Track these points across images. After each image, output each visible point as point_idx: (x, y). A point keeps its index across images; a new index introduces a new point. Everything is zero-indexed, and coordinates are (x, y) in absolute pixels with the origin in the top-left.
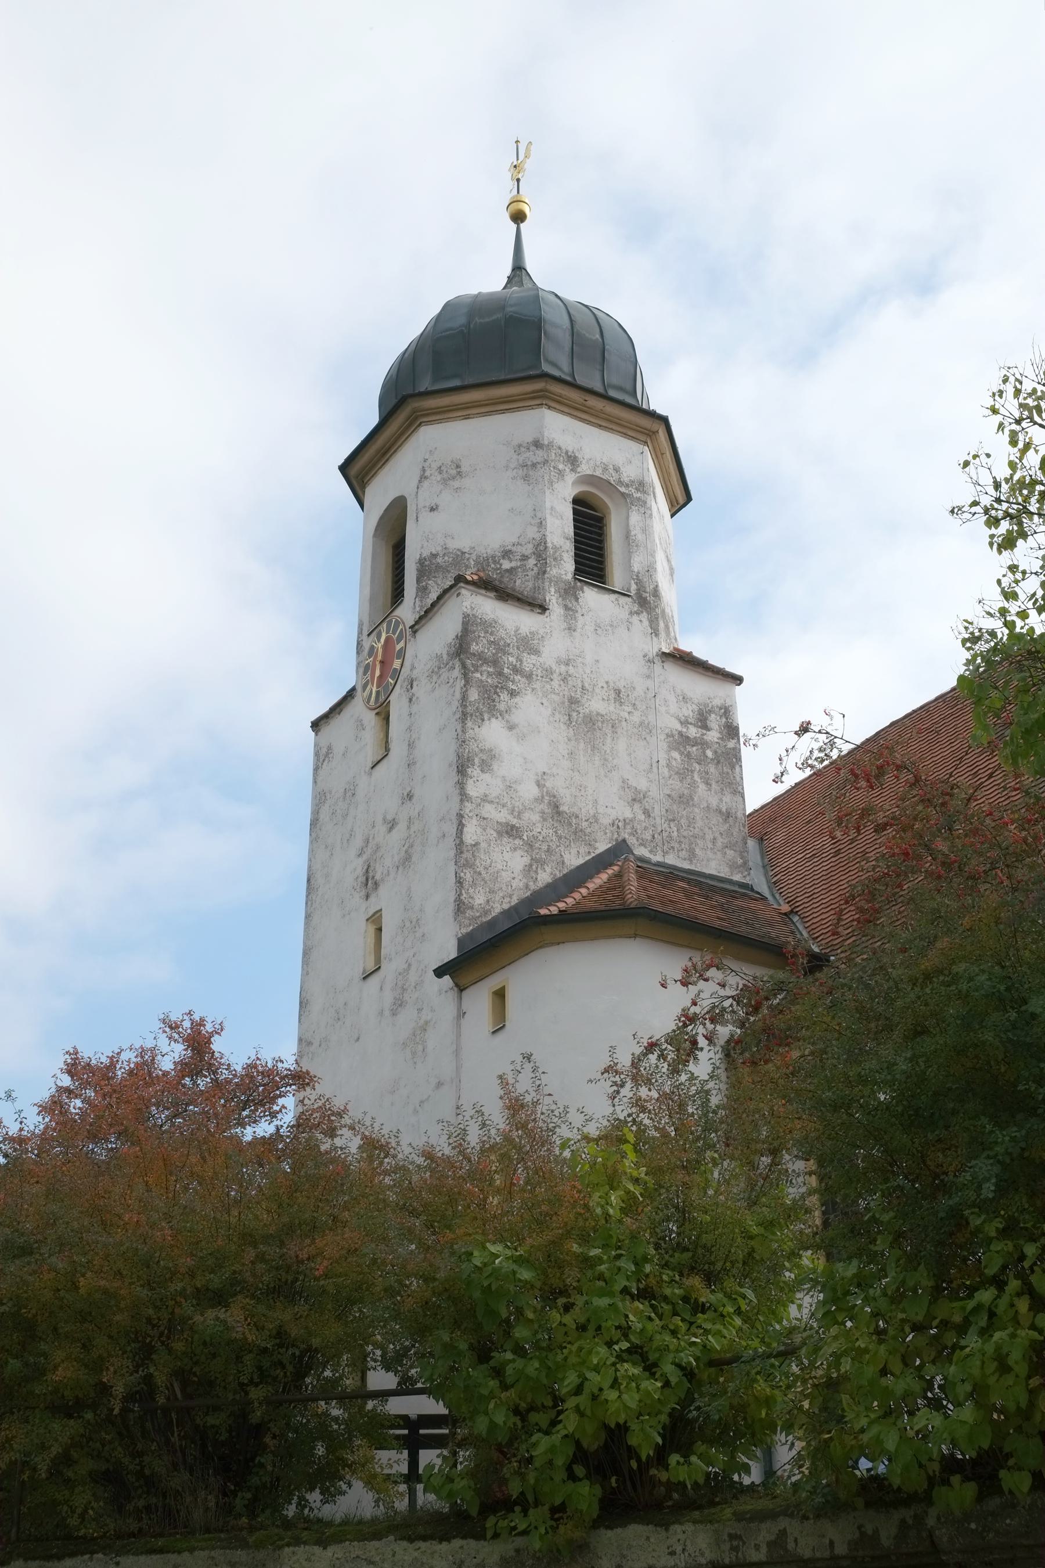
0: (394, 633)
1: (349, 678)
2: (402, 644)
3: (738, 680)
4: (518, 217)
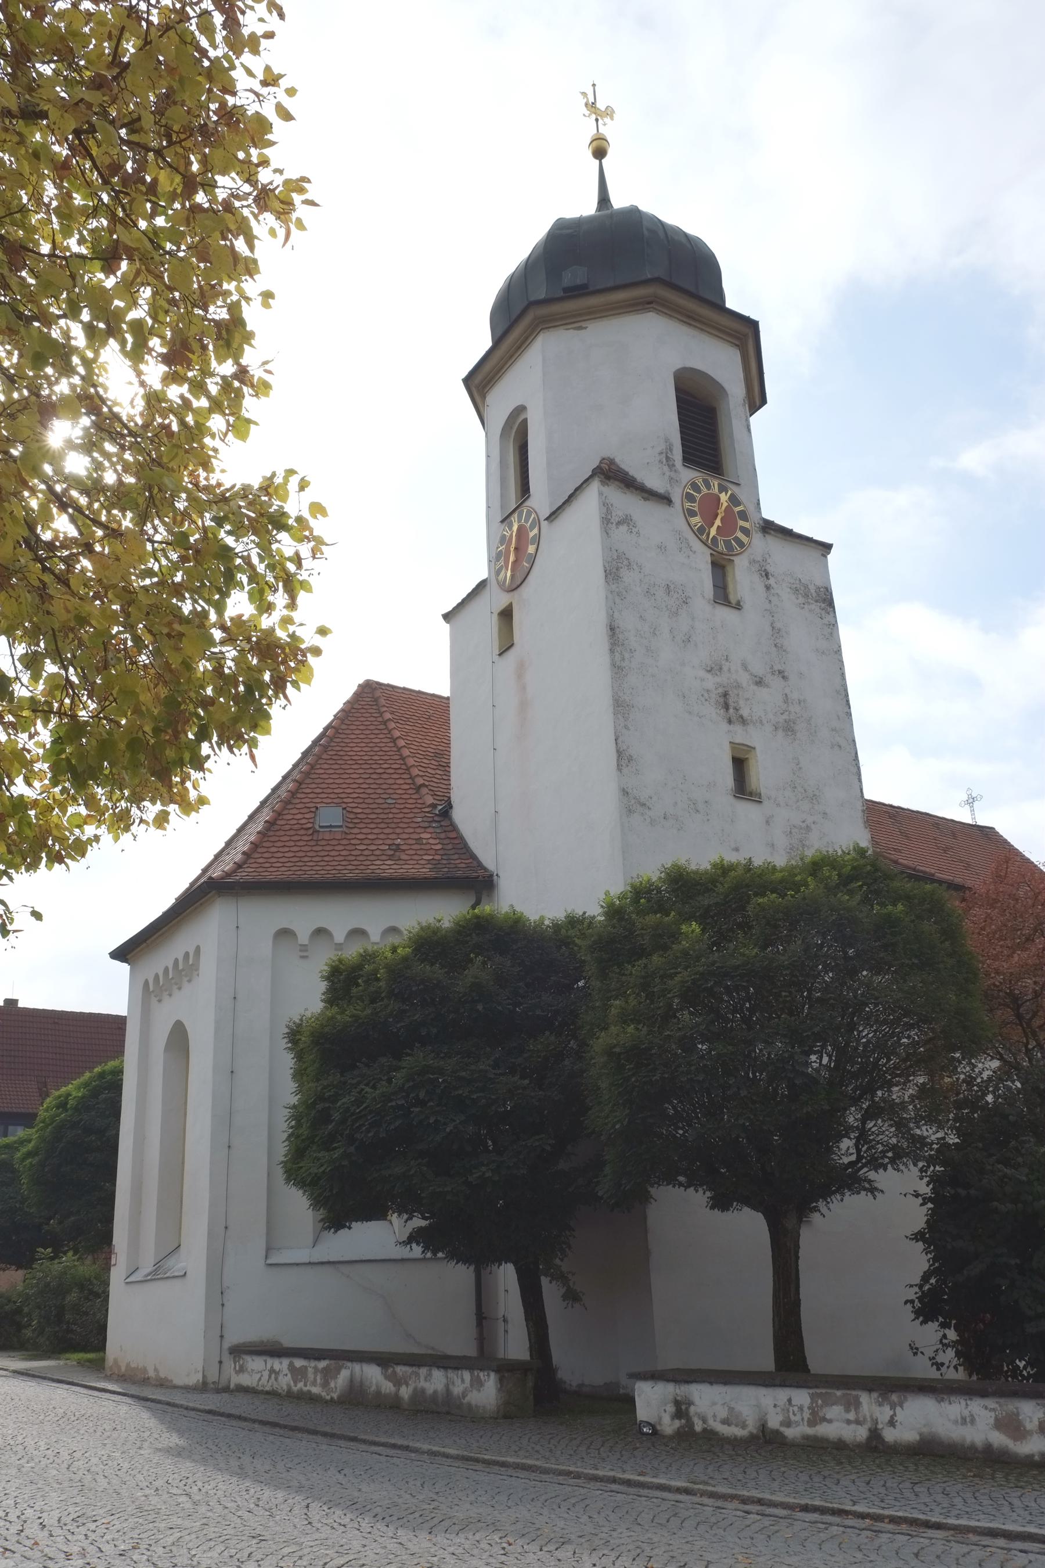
0: (526, 521)
1: (481, 571)
2: (535, 531)
3: (827, 547)
4: (600, 153)
